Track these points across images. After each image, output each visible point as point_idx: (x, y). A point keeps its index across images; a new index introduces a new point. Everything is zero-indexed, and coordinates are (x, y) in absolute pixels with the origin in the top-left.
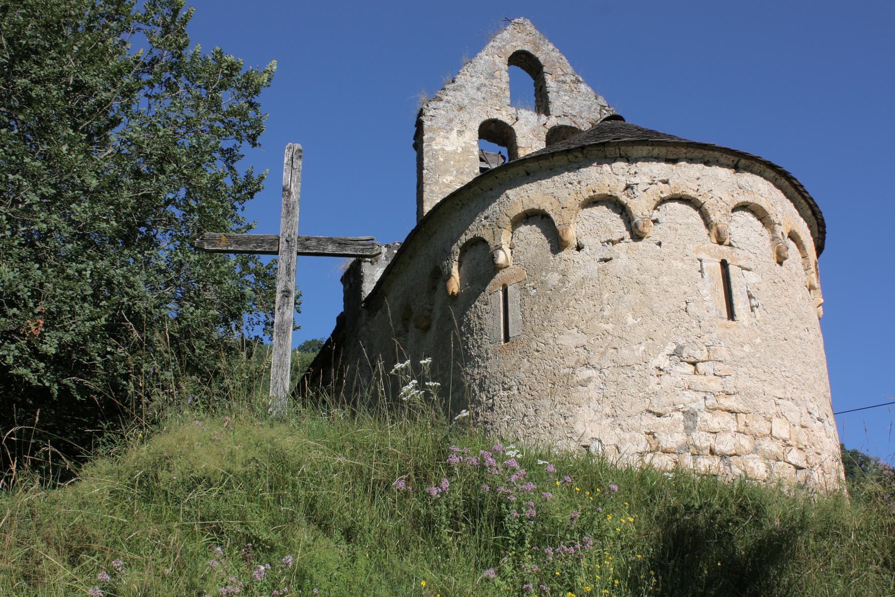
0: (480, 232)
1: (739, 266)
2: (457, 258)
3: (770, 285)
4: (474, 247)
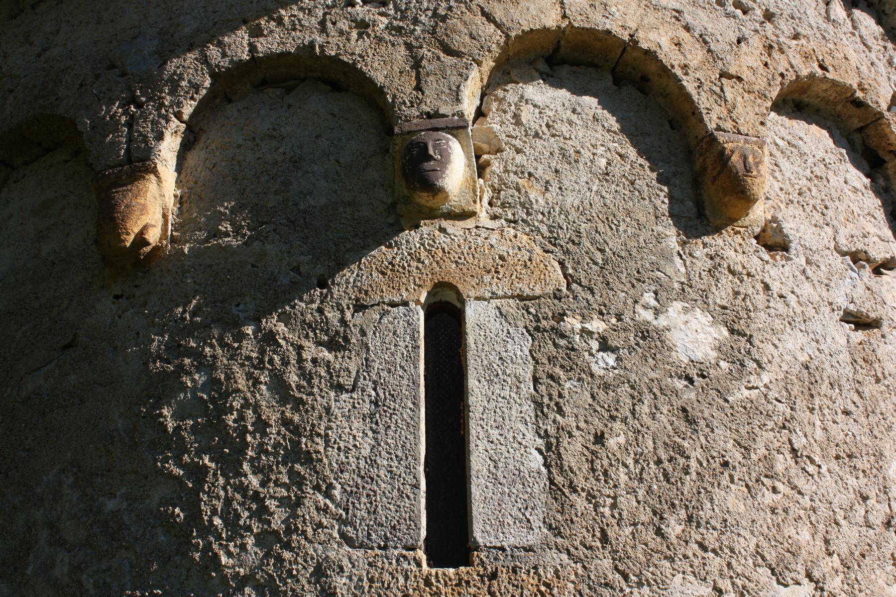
0: (335, 40)
2: (188, 109)
4: (273, 92)
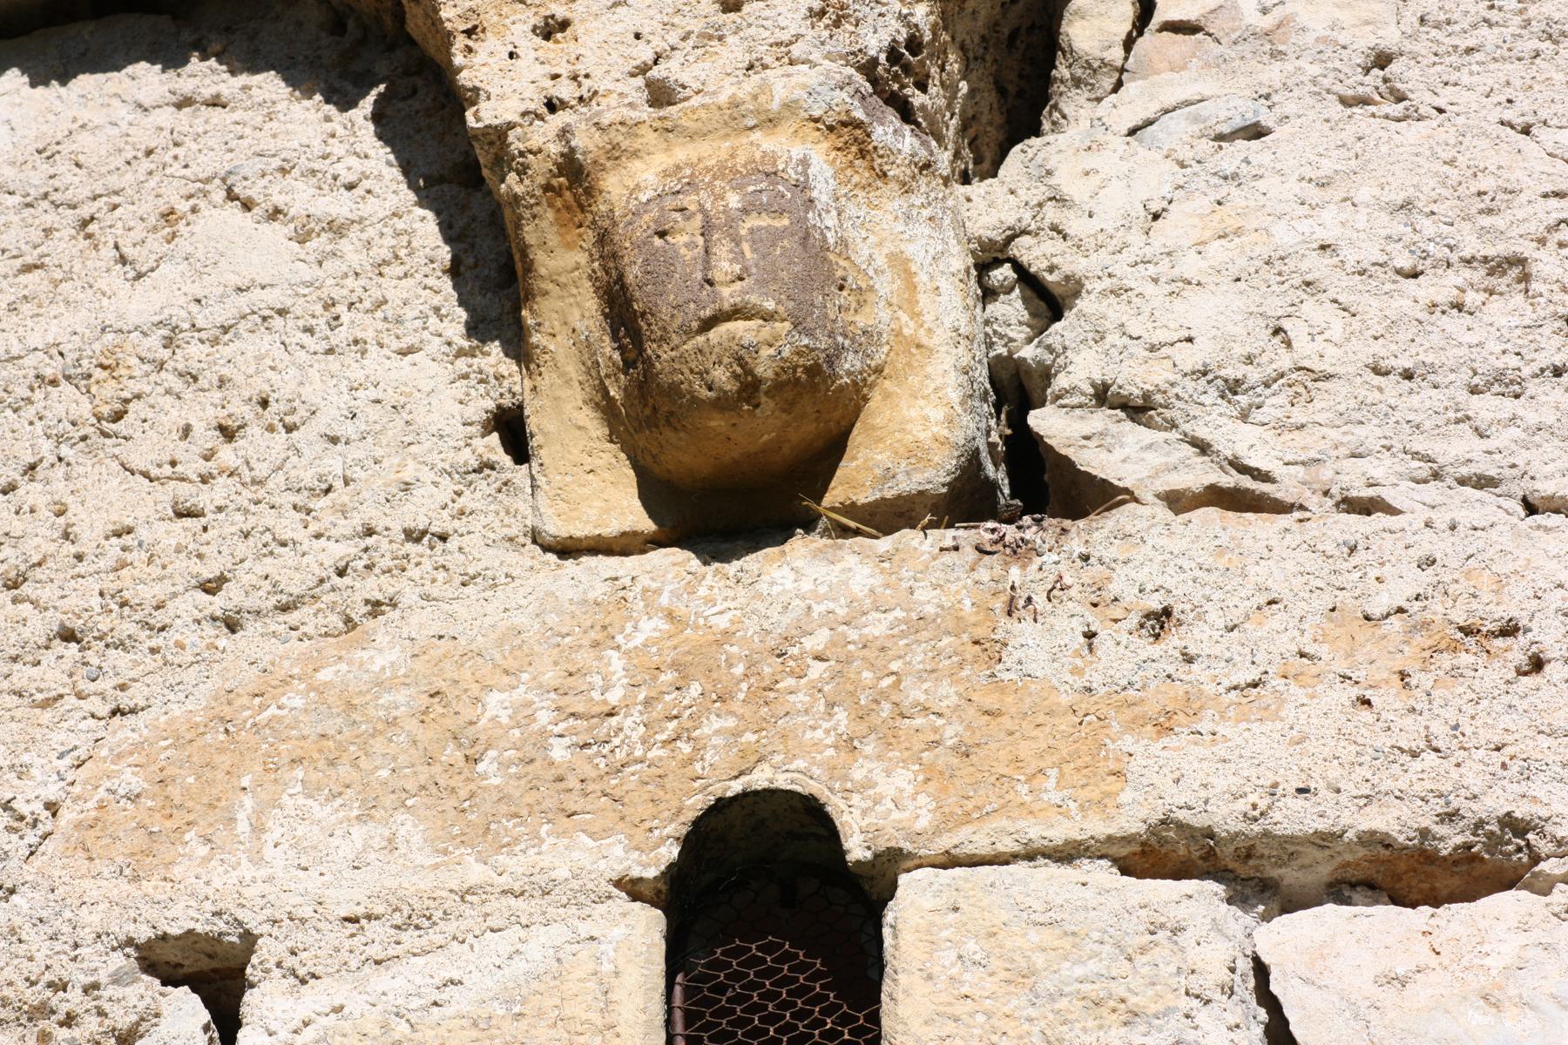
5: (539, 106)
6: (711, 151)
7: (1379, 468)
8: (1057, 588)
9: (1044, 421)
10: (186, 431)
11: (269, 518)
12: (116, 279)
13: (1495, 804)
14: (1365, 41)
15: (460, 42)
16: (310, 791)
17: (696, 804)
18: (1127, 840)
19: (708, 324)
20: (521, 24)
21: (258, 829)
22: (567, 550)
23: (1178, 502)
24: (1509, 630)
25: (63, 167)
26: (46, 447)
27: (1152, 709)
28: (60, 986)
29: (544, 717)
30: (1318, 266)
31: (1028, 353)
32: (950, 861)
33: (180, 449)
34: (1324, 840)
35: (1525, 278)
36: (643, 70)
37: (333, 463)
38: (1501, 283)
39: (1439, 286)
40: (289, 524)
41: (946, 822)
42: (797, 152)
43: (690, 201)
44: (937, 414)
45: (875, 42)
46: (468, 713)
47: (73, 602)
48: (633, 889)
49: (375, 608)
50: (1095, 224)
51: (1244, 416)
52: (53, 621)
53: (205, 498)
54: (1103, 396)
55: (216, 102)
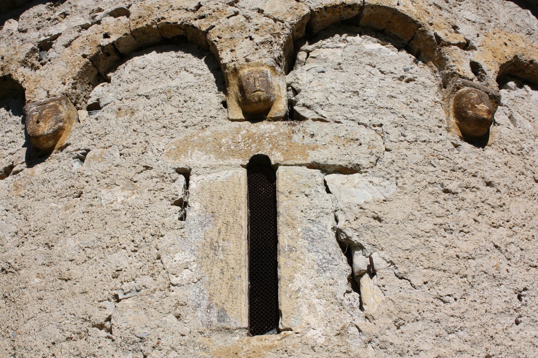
1: (312, 166)
3: (426, 200)
5: (230, 61)
6: (255, 69)
7: (340, 117)
8: (299, 130)
9: (296, 108)
10: (180, 101)
11: (191, 113)
12: (170, 80)
13: (356, 162)
14: (337, 61)
15: (220, 52)
16: (198, 150)
17: (251, 155)
18: (309, 164)
19: (255, 92)
20: (228, 50)
21: (191, 155)
22: (233, 120)
23: (314, 120)
24: (357, 140)
25: (162, 64)
26: (161, 102)
27: (312, 147)
28: (165, 173)
29: (230, 142)
30: (332, 90)
31: (293, 98)
32: (285, 165)
33: (179, 103)
34: (334, 165)
35: (358, 94)
36: (245, 57)
37: (200, 107)
38: (355, 94)
39: (348, 94)
40: (194, 115)
41: (285, 160)
42: (266, 70)
43: (252, 75)
44: (283, 106)
45: (276, 56)
46: (220, 141)
47: (165, 123)
48: (243, 166)
49: (207, 126)
50: (302, 83)
51: (322, 109)
52: (162, 125)
53: (182, 110)
54: (304, 105)
55: (182, 57)
